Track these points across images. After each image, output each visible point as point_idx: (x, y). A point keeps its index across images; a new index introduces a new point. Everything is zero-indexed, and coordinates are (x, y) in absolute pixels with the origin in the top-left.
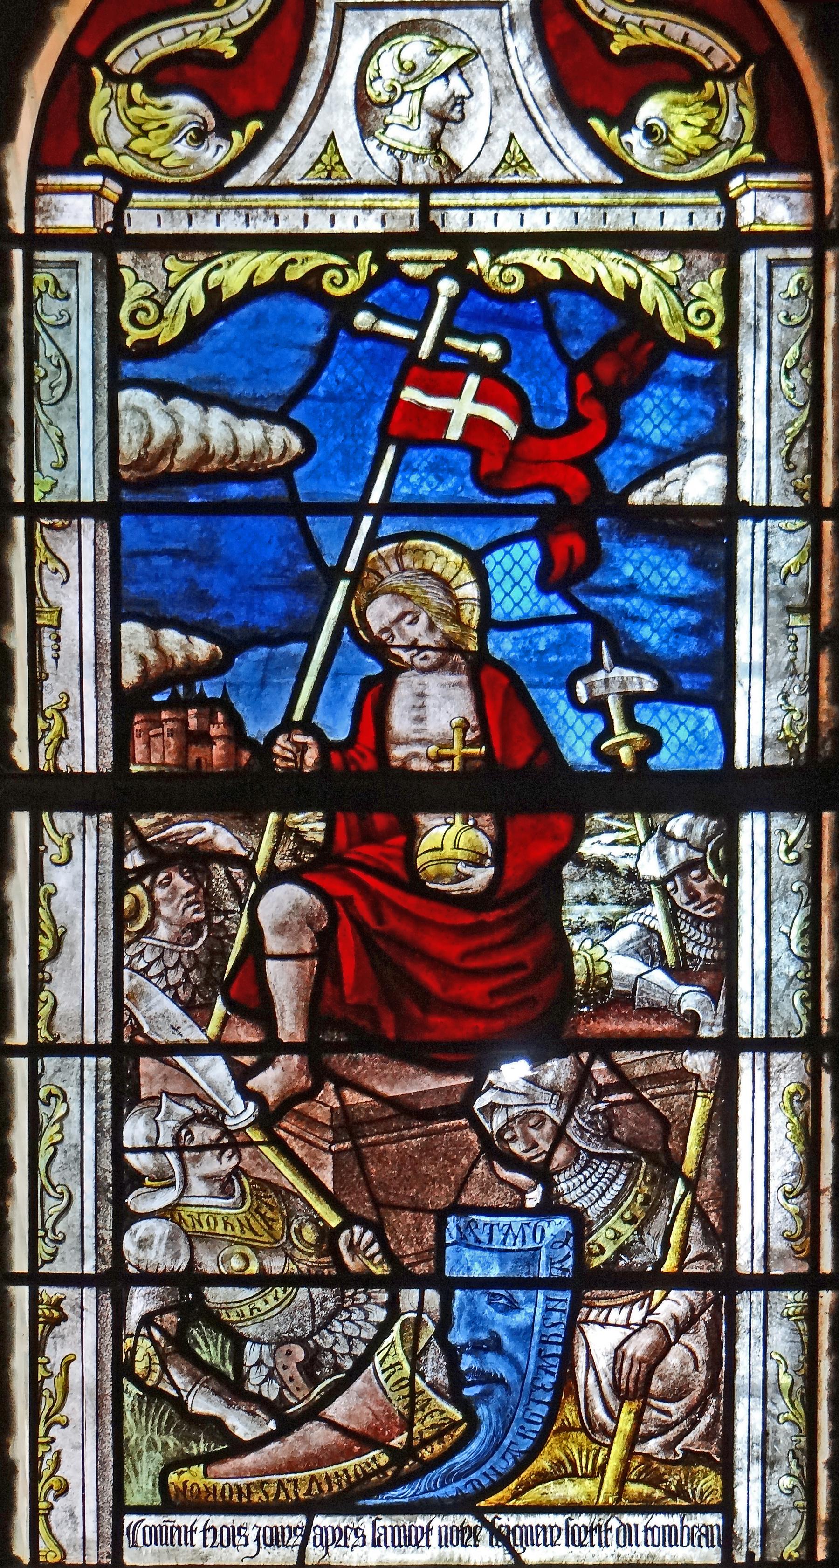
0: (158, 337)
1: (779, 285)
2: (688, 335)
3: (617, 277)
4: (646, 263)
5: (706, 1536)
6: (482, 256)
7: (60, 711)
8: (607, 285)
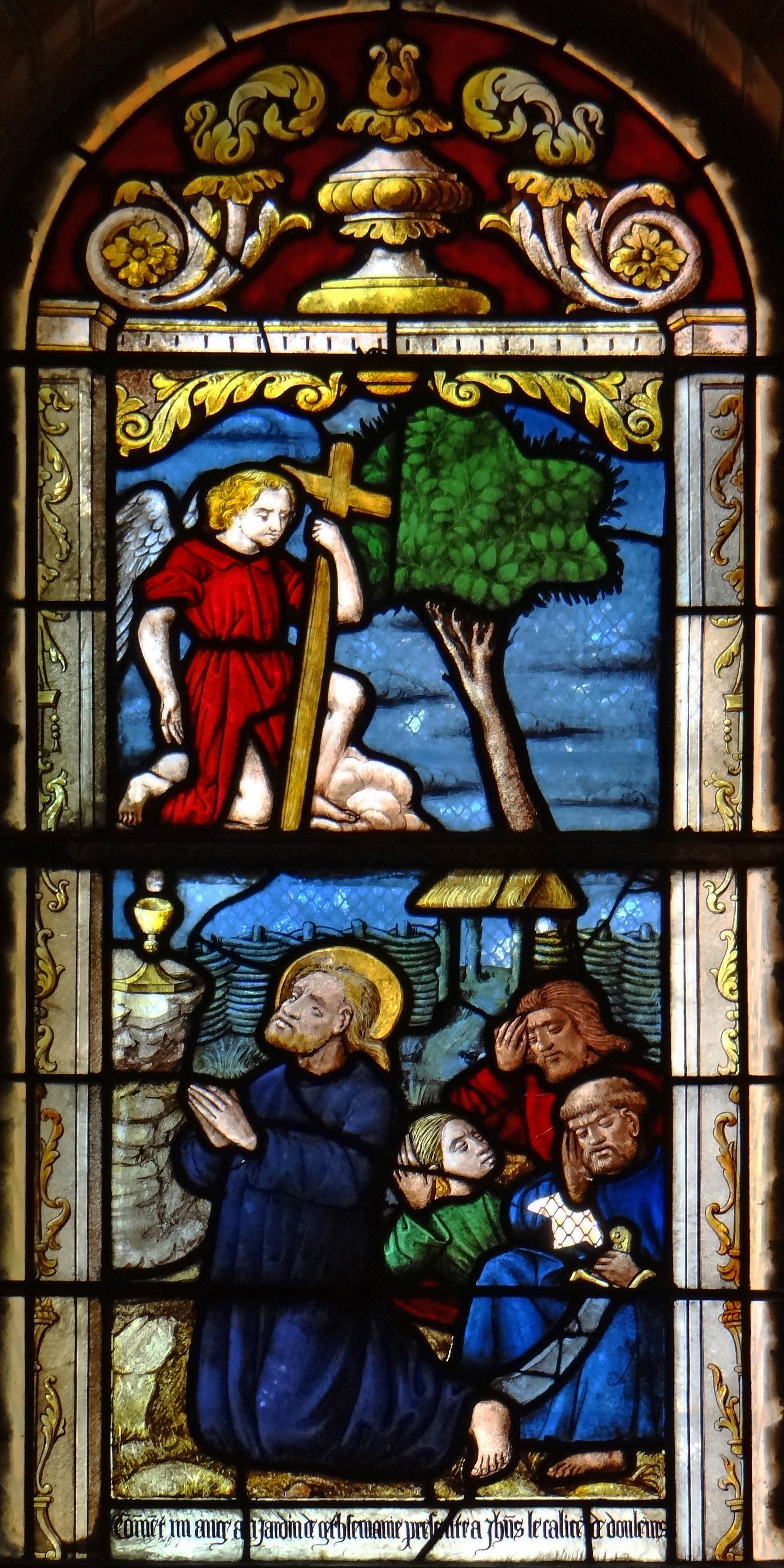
0: (148, 445)
2: (631, 443)
3: (565, 395)
6: (440, 376)
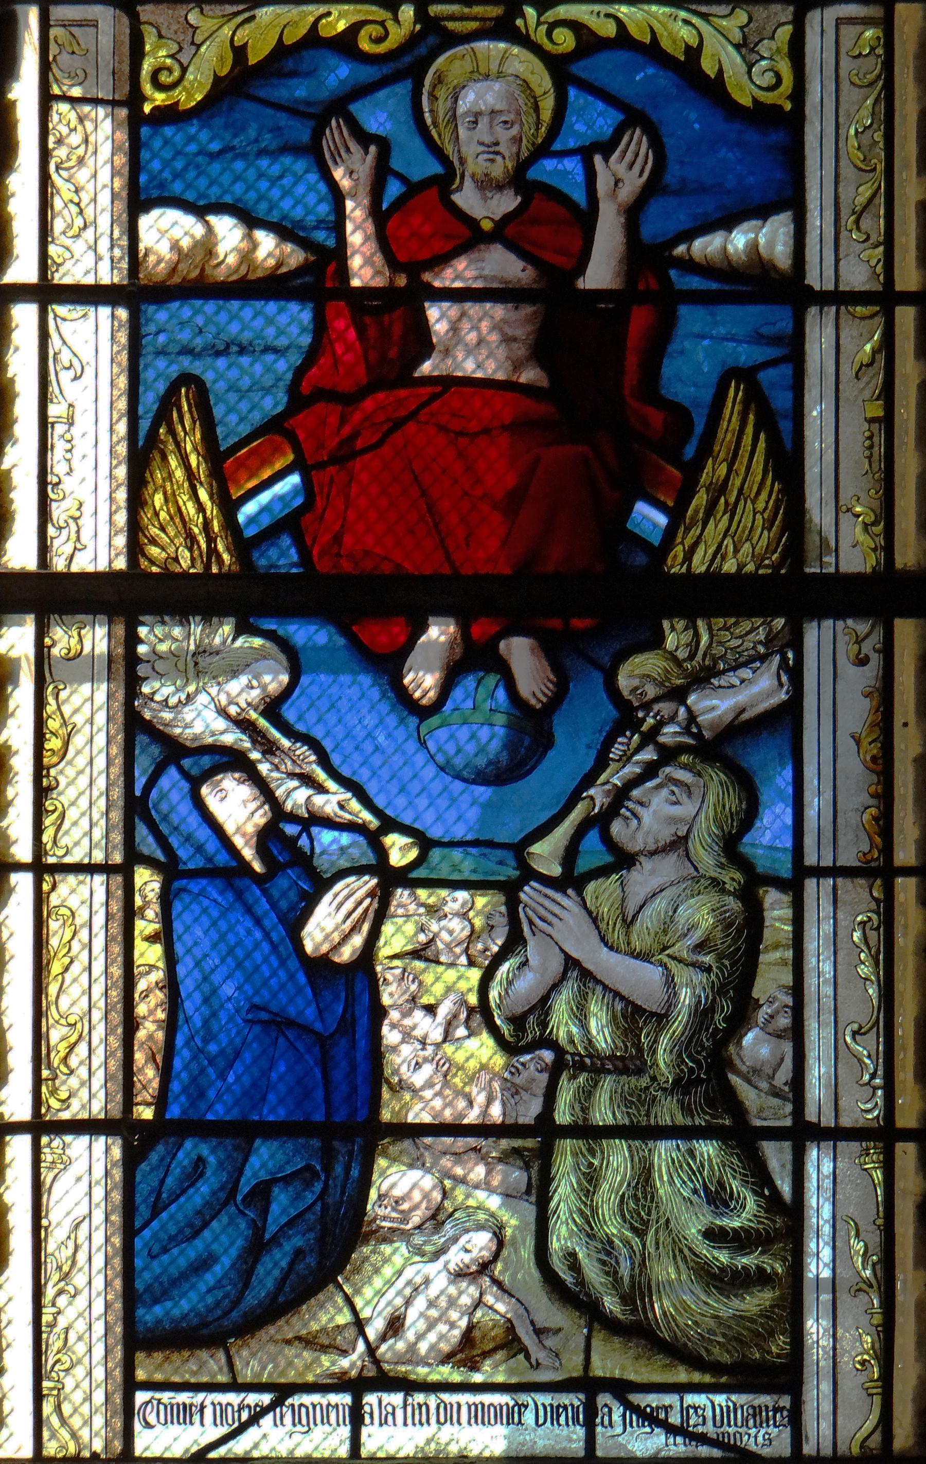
1: (846, 45)
4: (705, 17)
5: (754, 1416)
7: (75, 519)
8: (665, 44)
